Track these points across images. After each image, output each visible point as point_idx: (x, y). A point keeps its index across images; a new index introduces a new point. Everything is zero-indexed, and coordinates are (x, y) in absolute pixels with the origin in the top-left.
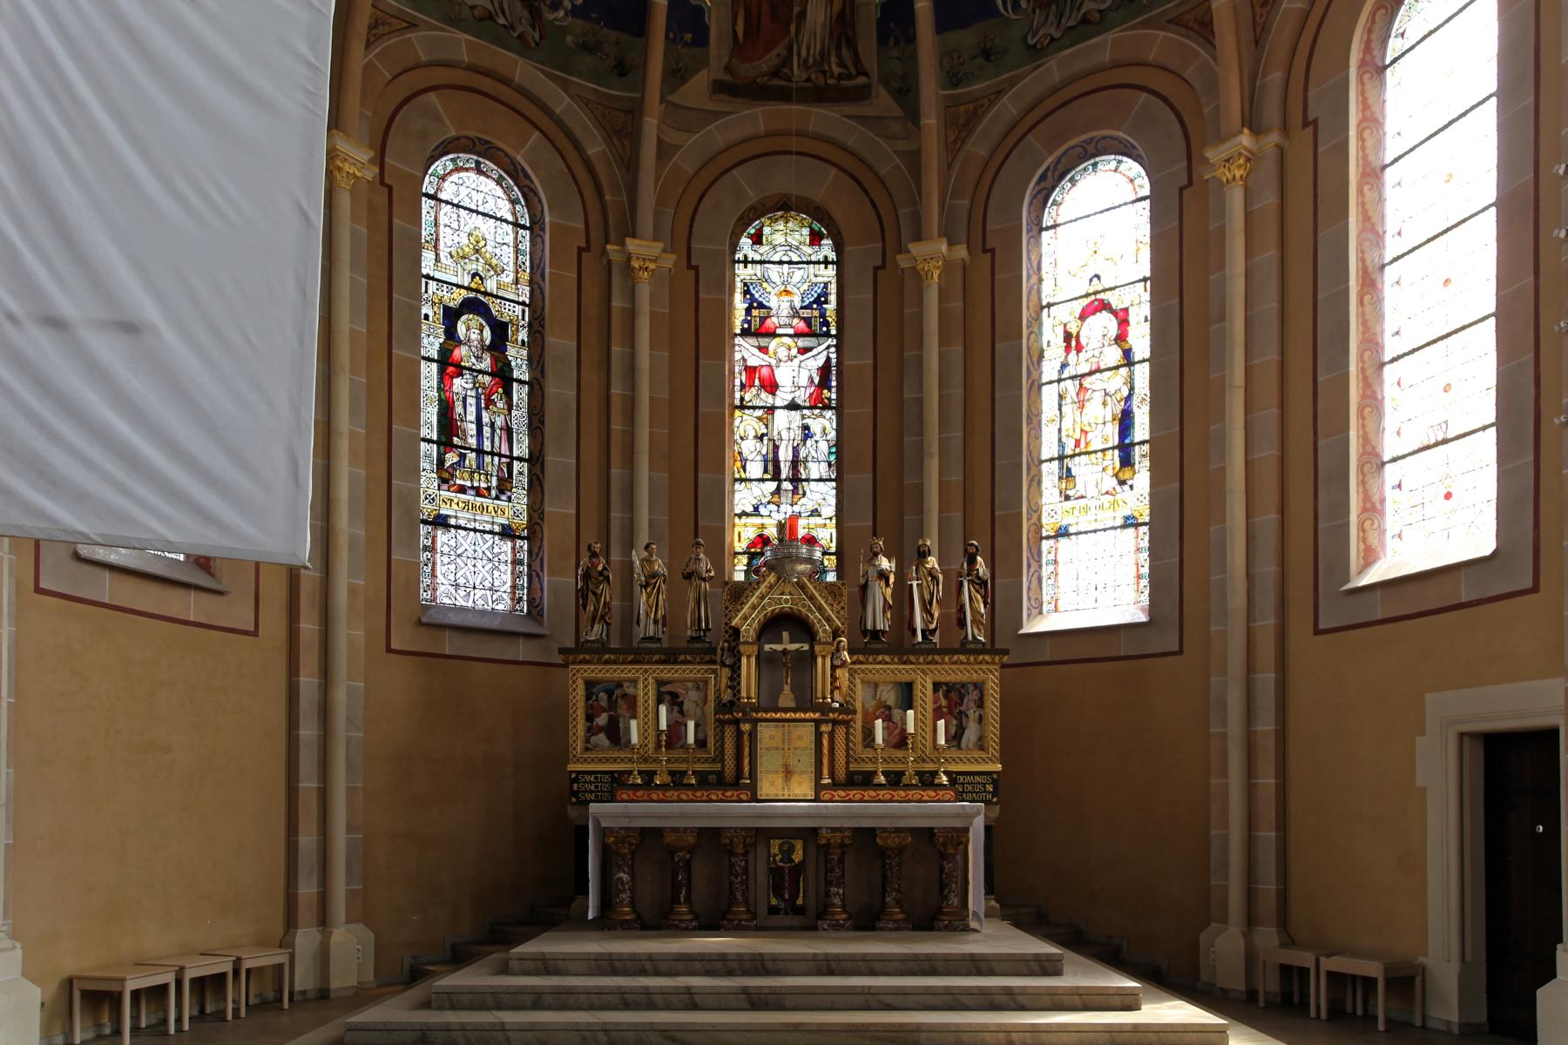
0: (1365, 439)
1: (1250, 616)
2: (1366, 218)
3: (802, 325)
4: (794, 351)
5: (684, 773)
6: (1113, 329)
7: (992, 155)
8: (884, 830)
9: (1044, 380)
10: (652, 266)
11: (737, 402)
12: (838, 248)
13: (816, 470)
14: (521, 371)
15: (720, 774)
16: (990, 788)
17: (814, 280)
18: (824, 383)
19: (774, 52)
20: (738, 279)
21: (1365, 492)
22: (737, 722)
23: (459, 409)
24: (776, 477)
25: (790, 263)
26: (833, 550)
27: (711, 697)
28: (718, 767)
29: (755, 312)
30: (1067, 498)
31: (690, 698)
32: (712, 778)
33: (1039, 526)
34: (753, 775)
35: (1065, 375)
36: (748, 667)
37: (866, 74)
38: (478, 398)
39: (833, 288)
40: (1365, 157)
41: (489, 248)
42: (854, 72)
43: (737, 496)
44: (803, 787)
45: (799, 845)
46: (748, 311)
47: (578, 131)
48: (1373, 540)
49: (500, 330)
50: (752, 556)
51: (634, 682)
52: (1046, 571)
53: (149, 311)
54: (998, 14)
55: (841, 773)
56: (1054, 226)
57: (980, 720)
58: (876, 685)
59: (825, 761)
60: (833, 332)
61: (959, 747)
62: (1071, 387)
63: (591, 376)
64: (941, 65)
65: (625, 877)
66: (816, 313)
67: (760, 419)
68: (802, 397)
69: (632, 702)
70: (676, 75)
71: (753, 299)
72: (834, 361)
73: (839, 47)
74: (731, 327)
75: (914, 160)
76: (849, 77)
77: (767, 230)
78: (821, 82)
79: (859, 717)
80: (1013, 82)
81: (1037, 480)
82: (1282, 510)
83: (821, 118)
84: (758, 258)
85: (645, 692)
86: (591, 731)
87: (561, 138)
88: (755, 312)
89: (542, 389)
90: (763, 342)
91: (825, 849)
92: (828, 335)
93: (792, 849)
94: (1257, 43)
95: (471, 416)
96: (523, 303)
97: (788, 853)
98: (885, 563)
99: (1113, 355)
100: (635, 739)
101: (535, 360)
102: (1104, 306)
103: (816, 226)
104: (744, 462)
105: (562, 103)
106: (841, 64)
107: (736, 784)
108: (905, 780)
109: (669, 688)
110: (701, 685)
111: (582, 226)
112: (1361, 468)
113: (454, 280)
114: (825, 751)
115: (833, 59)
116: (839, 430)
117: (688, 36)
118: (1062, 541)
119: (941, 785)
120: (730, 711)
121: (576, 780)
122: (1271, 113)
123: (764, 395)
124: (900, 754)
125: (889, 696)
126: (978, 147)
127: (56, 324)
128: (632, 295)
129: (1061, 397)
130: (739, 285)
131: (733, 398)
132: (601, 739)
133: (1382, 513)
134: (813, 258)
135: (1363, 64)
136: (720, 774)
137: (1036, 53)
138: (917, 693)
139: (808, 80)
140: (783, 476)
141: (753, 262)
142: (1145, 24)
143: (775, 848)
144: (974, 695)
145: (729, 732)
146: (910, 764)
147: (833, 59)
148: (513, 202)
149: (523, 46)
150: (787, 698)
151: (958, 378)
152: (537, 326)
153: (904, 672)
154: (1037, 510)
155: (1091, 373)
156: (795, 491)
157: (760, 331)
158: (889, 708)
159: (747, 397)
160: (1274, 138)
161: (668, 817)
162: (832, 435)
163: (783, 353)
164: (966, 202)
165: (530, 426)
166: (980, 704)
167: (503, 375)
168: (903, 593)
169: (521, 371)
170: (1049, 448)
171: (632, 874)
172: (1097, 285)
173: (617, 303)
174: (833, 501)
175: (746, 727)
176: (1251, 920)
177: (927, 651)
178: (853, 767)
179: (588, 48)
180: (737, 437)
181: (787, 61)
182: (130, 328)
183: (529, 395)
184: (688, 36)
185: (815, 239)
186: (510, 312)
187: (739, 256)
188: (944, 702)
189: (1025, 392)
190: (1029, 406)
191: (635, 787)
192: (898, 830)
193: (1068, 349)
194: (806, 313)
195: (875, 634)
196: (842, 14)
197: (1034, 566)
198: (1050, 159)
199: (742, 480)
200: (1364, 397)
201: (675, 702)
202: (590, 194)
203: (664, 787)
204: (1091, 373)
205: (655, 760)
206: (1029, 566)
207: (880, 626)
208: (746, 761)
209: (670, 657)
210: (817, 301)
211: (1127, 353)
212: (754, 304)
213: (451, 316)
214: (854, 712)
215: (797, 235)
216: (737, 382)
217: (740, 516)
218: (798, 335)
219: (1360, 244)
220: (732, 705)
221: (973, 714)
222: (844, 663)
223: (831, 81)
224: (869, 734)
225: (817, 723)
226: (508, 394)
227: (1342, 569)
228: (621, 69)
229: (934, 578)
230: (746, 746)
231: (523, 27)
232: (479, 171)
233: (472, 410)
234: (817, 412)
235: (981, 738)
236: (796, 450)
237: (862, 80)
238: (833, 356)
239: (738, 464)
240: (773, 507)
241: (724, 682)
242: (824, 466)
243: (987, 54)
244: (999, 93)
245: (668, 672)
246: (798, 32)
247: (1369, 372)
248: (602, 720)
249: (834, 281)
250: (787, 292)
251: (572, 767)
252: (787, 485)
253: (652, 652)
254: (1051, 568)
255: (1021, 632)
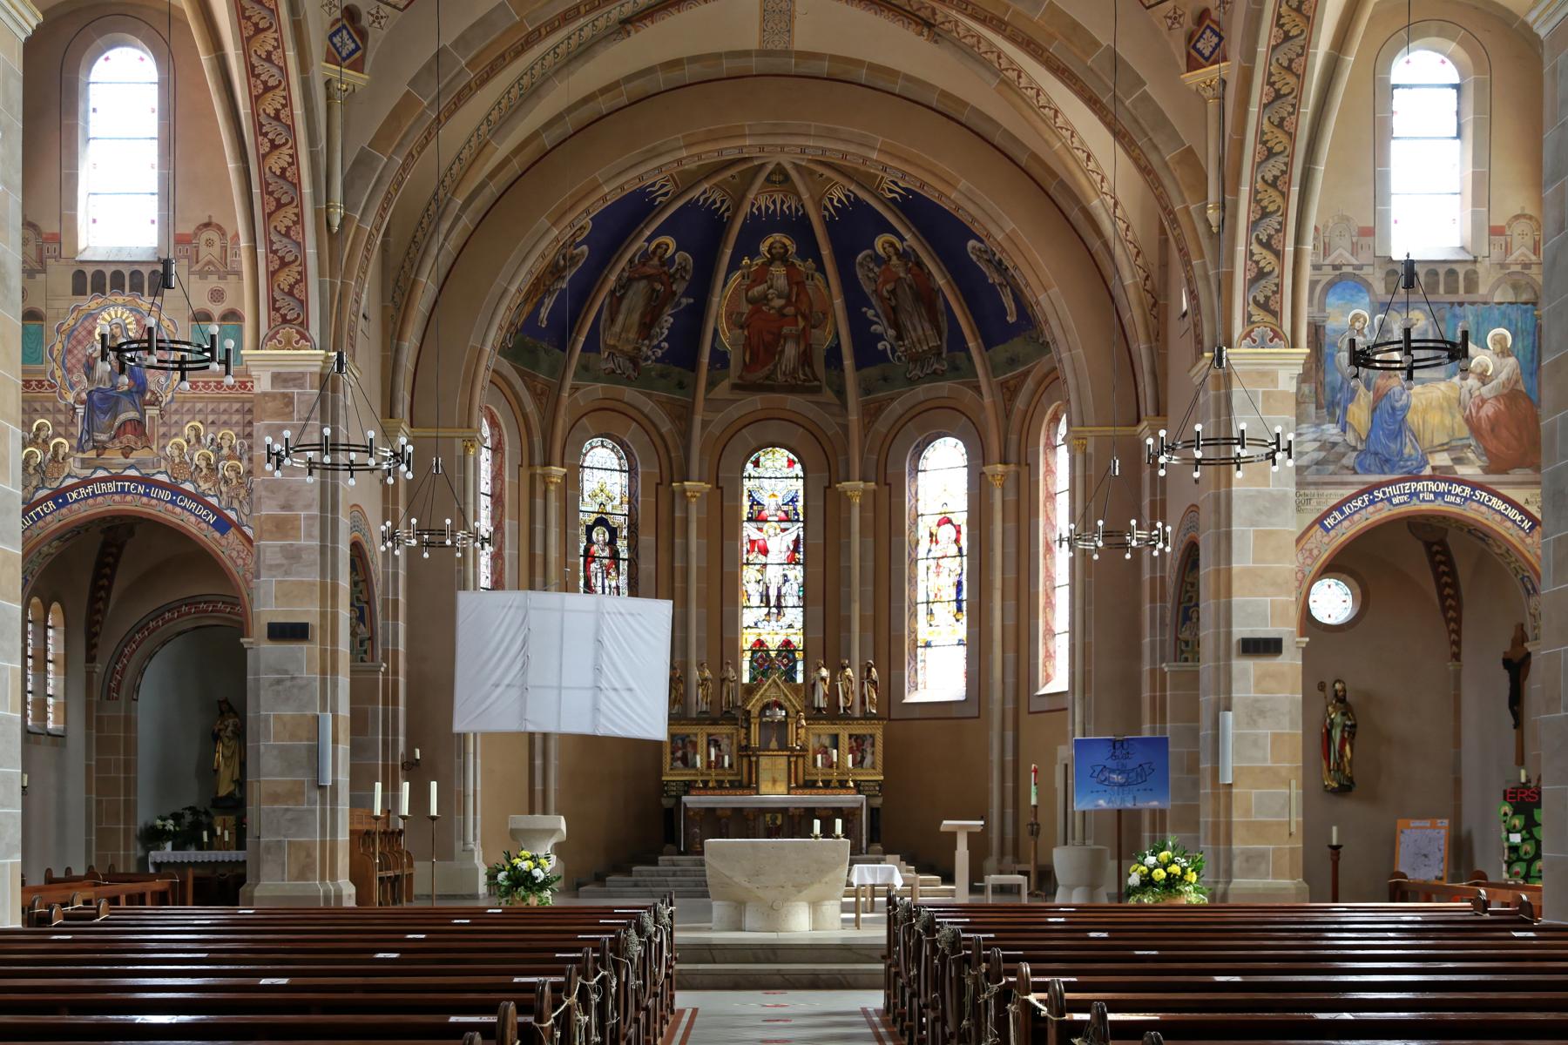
0: (1047, 623)
1: (1003, 703)
2: (1048, 518)
3: (783, 515)
4: (778, 531)
5: (723, 782)
6: (953, 535)
7: (889, 432)
8: (819, 808)
9: (919, 557)
10: (698, 495)
11: (745, 561)
12: (804, 469)
13: (791, 599)
14: (624, 554)
15: (740, 782)
16: (877, 788)
17: (790, 488)
18: (796, 550)
19: (766, 368)
20: (745, 488)
21: (1047, 648)
22: (749, 756)
23: (593, 581)
24: (768, 605)
25: (776, 478)
26: (801, 648)
27: (735, 741)
28: (739, 778)
29: (755, 508)
30: (931, 625)
31: (724, 744)
32: (737, 784)
33: (916, 640)
34: (757, 782)
35: (931, 555)
36: (755, 730)
37: (819, 380)
38: (603, 573)
39: (801, 493)
40: (1047, 489)
41: (608, 488)
42: (811, 378)
43: (744, 616)
44: (782, 788)
45: (780, 816)
46: (751, 507)
47: (657, 422)
48: (1050, 671)
49: (613, 532)
50: (754, 652)
51: (696, 735)
52: (920, 665)
53: (634, 685)
54: (889, 360)
55: (801, 782)
56: (924, 471)
57: (873, 753)
58: (819, 736)
59: (793, 775)
60: (801, 519)
61: (862, 767)
62: (932, 563)
63: (664, 557)
64: (860, 385)
65: (698, 831)
66: (791, 508)
67: (758, 571)
68: (783, 558)
69: (694, 745)
70: (711, 384)
71: (754, 500)
72: (802, 536)
73: (803, 366)
74: (741, 515)
75: (845, 428)
76: (810, 381)
77: (762, 459)
78: (793, 382)
79: (811, 752)
80: (900, 394)
81: (914, 615)
82: (1017, 651)
83: (793, 402)
84: (757, 475)
85: (702, 742)
86: (674, 759)
87: (647, 425)
88: (755, 508)
89: (636, 565)
90: (760, 525)
91: (792, 817)
92: (798, 521)
93: (776, 818)
94: (1007, 417)
95: (599, 584)
96: (625, 515)
97: (774, 820)
98: (824, 672)
99: (953, 550)
100: (699, 765)
101: (632, 547)
102: (949, 521)
103: (792, 456)
104: (749, 596)
105: (648, 406)
106: (805, 375)
107: (748, 787)
108: (832, 785)
109: (713, 737)
110: (730, 737)
111: (657, 471)
112: (1044, 637)
113: (591, 510)
114: (793, 771)
115: (800, 372)
116: (804, 577)
117: (718, 365)
118: (928, 649)
119: (850, 787)
120: (745, 751)
121: (666, 785)
122: (1013, 456)
123: (761, 556)
124: (830, 771)
125: (827, 741)
126: (882, 426)
127: (615, 689)
128: (686, 510)
129: (928, 568)
130: (746, 493)
131: (742, 558)
132: (679, 764)
133: (1054, 658)
134: (790, 475)
135: (1046, 445)
136: (740, 782)
137: (912, 382)
138: (841, 739)
139: (786, 381)
140: (772, 605)
141: (754, 478)
142: (963, 384)
143: (768, 817)
144: (870, 740)
145: (745, 761)
146: (835, 775)
147: (800, 372)
148: (620, 458)
149: (629, 381)
150: (774, 744)
151: (870, 556)
152: (633, 527)
153: (834, 729)
154: (914, 632)
155: (943, 557)
156: (779, 614)
157: (758, 519)
158: (826, 747)
159: (751, 558)
160: (1012, 467)
161: (719, 803)
162: (801, 580)
163: (771, 532)
164: (875, 457)
165: (629, 584)
166: (873, 745)
167: (615, 556)
168: (833, 689)
169: (624, 554)
170: (921, 597)
171: (700, 829)
172: (945, 509)
173: (678, 514)
174: (801, 619)
175: (754, 759)
176: (1002, 853)
177: (847, 718)
178: (807, 778)
179: (662, 376)
180: (744, 582)
181: (774, 372)
182: (630, 690)
183: (629, 566)
184: (718, 365)
185: (791, 463)
186: (619, 521)
187: (746, 474)
188: (854, 744)
189: (907, 566)
190: (909, 573)
191: (699, 788)
192: (826, 808)
193: (931, 541)
194: (785, 508)
195: (819, 709)
196: (805, 351)
197: (912, 663)
198: (920, 439)
199: (747, 607)
200: (1046, 603)
201: (717, 745)
202: (662, 452)
203: (714, 788)
204: (943, 557)
205: (710, 775)
206: (909, 663)
207: (822, 705)
208: (754, 775)
209: (714, 722)
210: (792, 500)
211: (960, 549)
212: (755, 502)
213: (590, 529)
214: (807, 751)
215: (779, 462)
216: (745, 549)
217: (746, 628)
218: (781, 521)
219: (1045, 530)
220: (747, 747)
221: (869, 750)
222: (802, 726)
223: (799, 383)
224: (815, 760)
225: (789, 756)
226: (617, 568)
227: (1032, 682)
228: (681, 385)
229: (850, 680)
230: (753, 768)
231: (630, 372)
232: (603, 446)
233: (600, 579)
234: (792, 566)
235: (873, 763)
236: (779, 589)
237: (816, 383)
238: (801, 534)
239: (746, 597)
240: (765, 623)
241: (742, 735)
242: (796, 598)
243: (885, 379)
244: (892, 399)
245: (712, 729)
246: (779, 359)
247: (1049, 591)
248: (679, 754)
249: (802, 488)
250: (774, 495)
251: (664, 778)
252: (774, 610)
253: (706, 719)
254: (923, 664)
255: (904, 701)
